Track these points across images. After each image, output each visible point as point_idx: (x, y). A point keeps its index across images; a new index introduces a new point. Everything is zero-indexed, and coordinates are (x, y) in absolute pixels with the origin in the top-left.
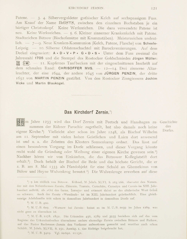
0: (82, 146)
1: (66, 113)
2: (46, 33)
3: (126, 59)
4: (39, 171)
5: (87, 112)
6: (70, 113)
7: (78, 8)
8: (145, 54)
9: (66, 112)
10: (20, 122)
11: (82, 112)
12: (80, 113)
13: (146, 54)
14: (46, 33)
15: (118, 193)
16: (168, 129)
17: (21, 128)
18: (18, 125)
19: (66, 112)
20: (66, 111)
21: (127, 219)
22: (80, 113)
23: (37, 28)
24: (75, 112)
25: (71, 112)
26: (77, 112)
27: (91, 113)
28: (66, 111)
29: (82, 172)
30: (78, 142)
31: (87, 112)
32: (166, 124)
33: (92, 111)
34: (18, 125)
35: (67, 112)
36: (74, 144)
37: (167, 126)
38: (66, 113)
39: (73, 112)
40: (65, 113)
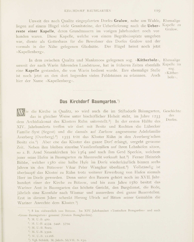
0: (106, 161)
1: (61, 102)
2: (109, 157)
3: (117, 162)
4: (82, 161)
5: (83, 102)
6: (65, 102)
7: (74, 11)
8: (148, 36)
9: (61, 101)
10: (21, 112)
11: (78, 102)
12: (75, 102)
13: (139, 71)
14: (109, 157)
15: (120, 119)
16: (171, 118)
17: (21, 118)
18: (18, 115)
19: (61, 101)
20: (61, 101)
21: (69, 24)
22: (75, 102)
23: (55, 66)
24: (71, 101)
25: (66, 102)
26: (72, 101)
27: (87, 102)
28: (61, 101)
29: (148, 182)
30: (64, 122)
31: (83, 102)
32: (169, 113)
33: (88, 101)
34: (18, 115)
35: (63, 102)
36: (123, 176)
37: (170, 115)
38: (61, 102)
39: (69, 102)
40: (60, 103)
